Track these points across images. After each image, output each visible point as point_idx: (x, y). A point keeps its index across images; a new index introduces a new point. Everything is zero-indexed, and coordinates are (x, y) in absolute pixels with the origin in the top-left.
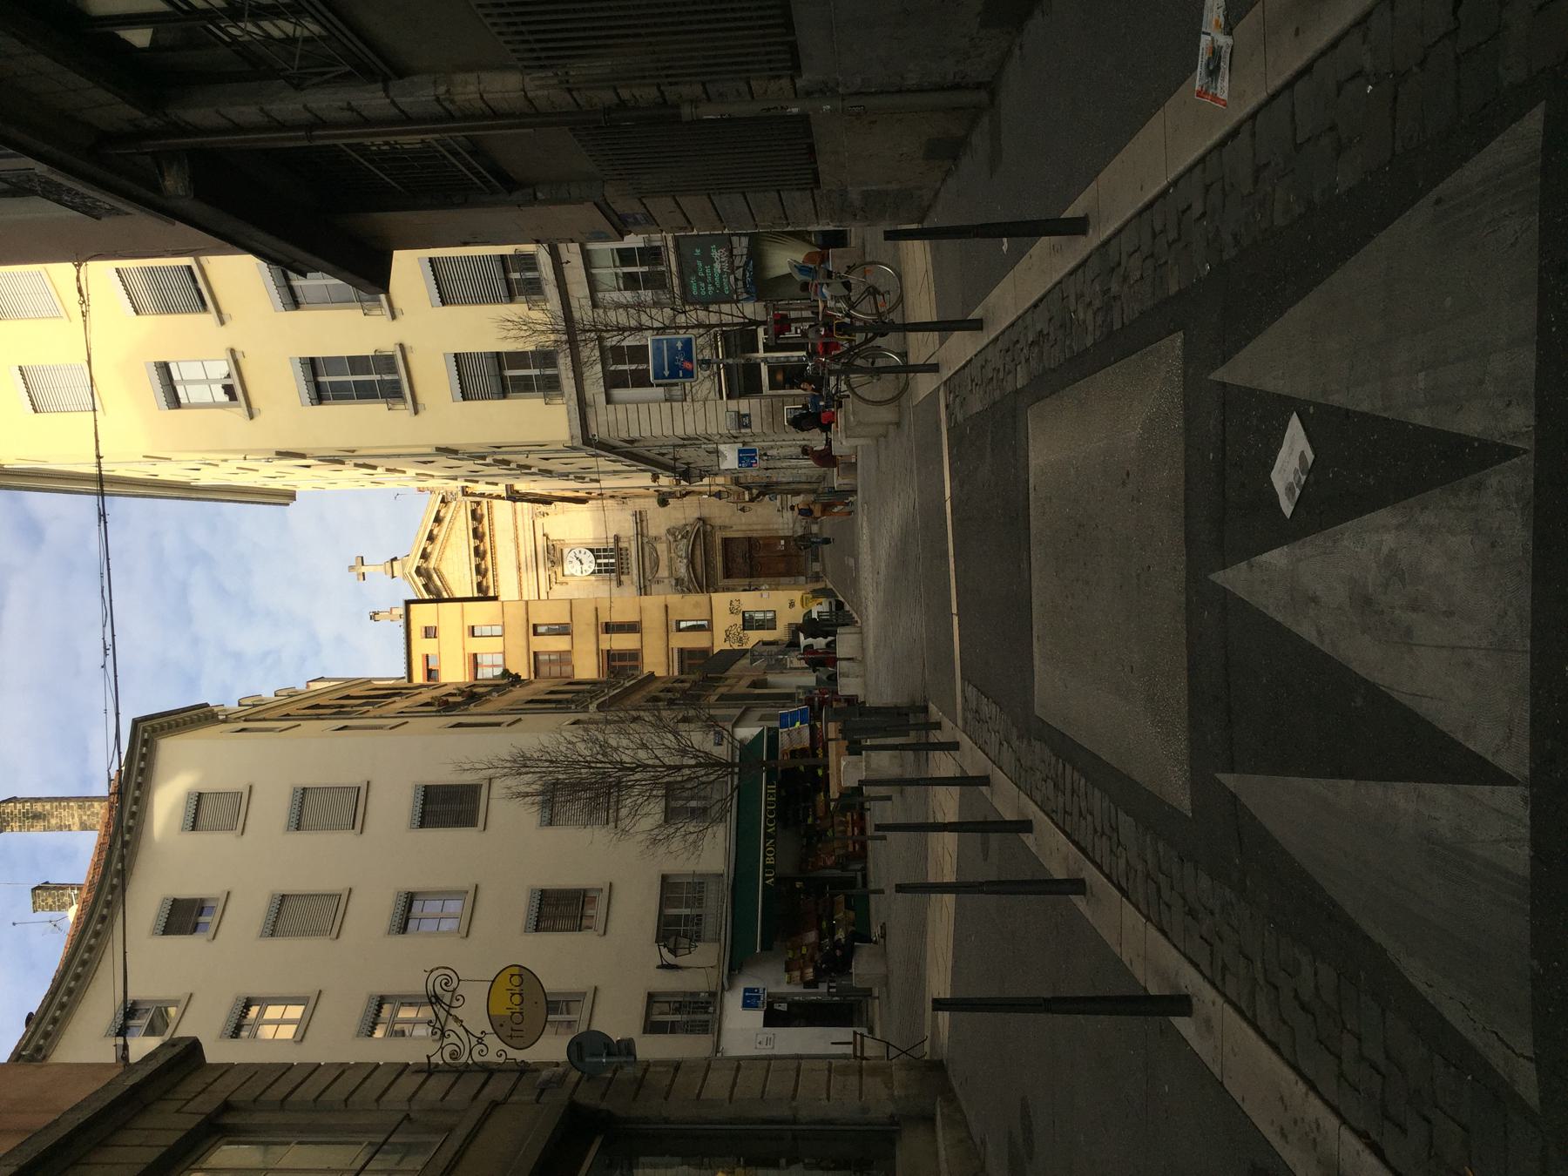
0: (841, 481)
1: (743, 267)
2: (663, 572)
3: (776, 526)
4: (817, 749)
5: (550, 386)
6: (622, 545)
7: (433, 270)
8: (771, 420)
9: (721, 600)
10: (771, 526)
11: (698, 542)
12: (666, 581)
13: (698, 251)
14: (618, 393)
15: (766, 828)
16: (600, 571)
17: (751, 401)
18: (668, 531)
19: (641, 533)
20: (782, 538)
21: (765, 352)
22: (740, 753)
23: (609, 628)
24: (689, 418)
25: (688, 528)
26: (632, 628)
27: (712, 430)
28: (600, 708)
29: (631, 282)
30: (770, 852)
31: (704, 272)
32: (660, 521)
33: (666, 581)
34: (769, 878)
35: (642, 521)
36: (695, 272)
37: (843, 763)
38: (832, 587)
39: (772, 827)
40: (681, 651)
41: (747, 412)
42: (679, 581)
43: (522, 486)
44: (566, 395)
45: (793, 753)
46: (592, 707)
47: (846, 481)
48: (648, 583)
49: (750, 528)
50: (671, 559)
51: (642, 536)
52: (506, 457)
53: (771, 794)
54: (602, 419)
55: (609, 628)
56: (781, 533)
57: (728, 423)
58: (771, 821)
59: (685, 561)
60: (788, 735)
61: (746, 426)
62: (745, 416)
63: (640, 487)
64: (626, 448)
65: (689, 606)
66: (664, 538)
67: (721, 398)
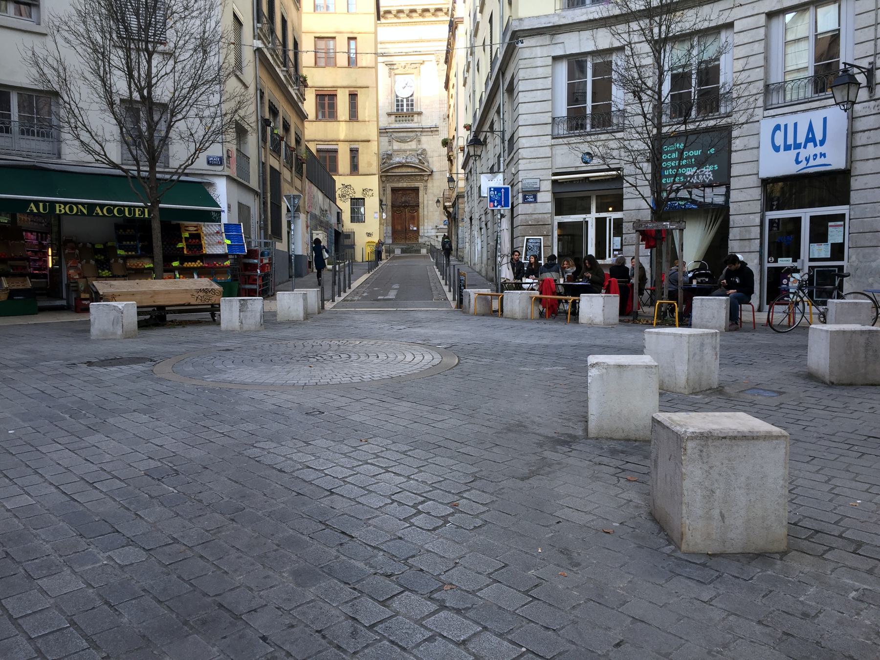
0: (473, 297)
1: (691, 198)
2: (396, 146)
3: (426, 224)
4: (202, 261)
6: (416, 116)
8: (530, 223)
9: (373, 183)
10: (426, 221)
11: (417, 170)
12: (390, 148)
14: (563, 68)
15: (102, 206)
16: (398, 101)
17: (550, 204)
18: (424, 150)
19: (423, 130)
20: (418, 228)
22: (166, 180)
23: (353, 96)
24: (535, 141)
25: (426, 164)
26: (353, 115)
27: (522, 165)
28: (258, 50)
29: (680, 80)
30: (71, 209)
32: (432, 146)
33: (390, 148)
34: (38, 208)
35: (432, 131)
37: (120, 305)
38: (380, 266)
39: (102, 212)
40: (336, 151)
41: (538, 200)
42: (389, 156)
43: (463, 32)
44: (564, 13)
45: (196, 237)
46: (259, 44)
47: (472, 301)
48: (389, 135)
49: (425, 208)
50: (405, 151)
51: (421, 131)
52: (471, 70)
53: (143, 213)
54: (538, 52)
55: (353, 96)
56: (421, 228)
57: (528, 181)
59: (404, 161)
60: (218, 232)
61: (524, 198)
62: (535, 197)
63: (457, 123)
64: (503, 85)
65: (369, 159)
66: (419, 147)
67: (555, 174)
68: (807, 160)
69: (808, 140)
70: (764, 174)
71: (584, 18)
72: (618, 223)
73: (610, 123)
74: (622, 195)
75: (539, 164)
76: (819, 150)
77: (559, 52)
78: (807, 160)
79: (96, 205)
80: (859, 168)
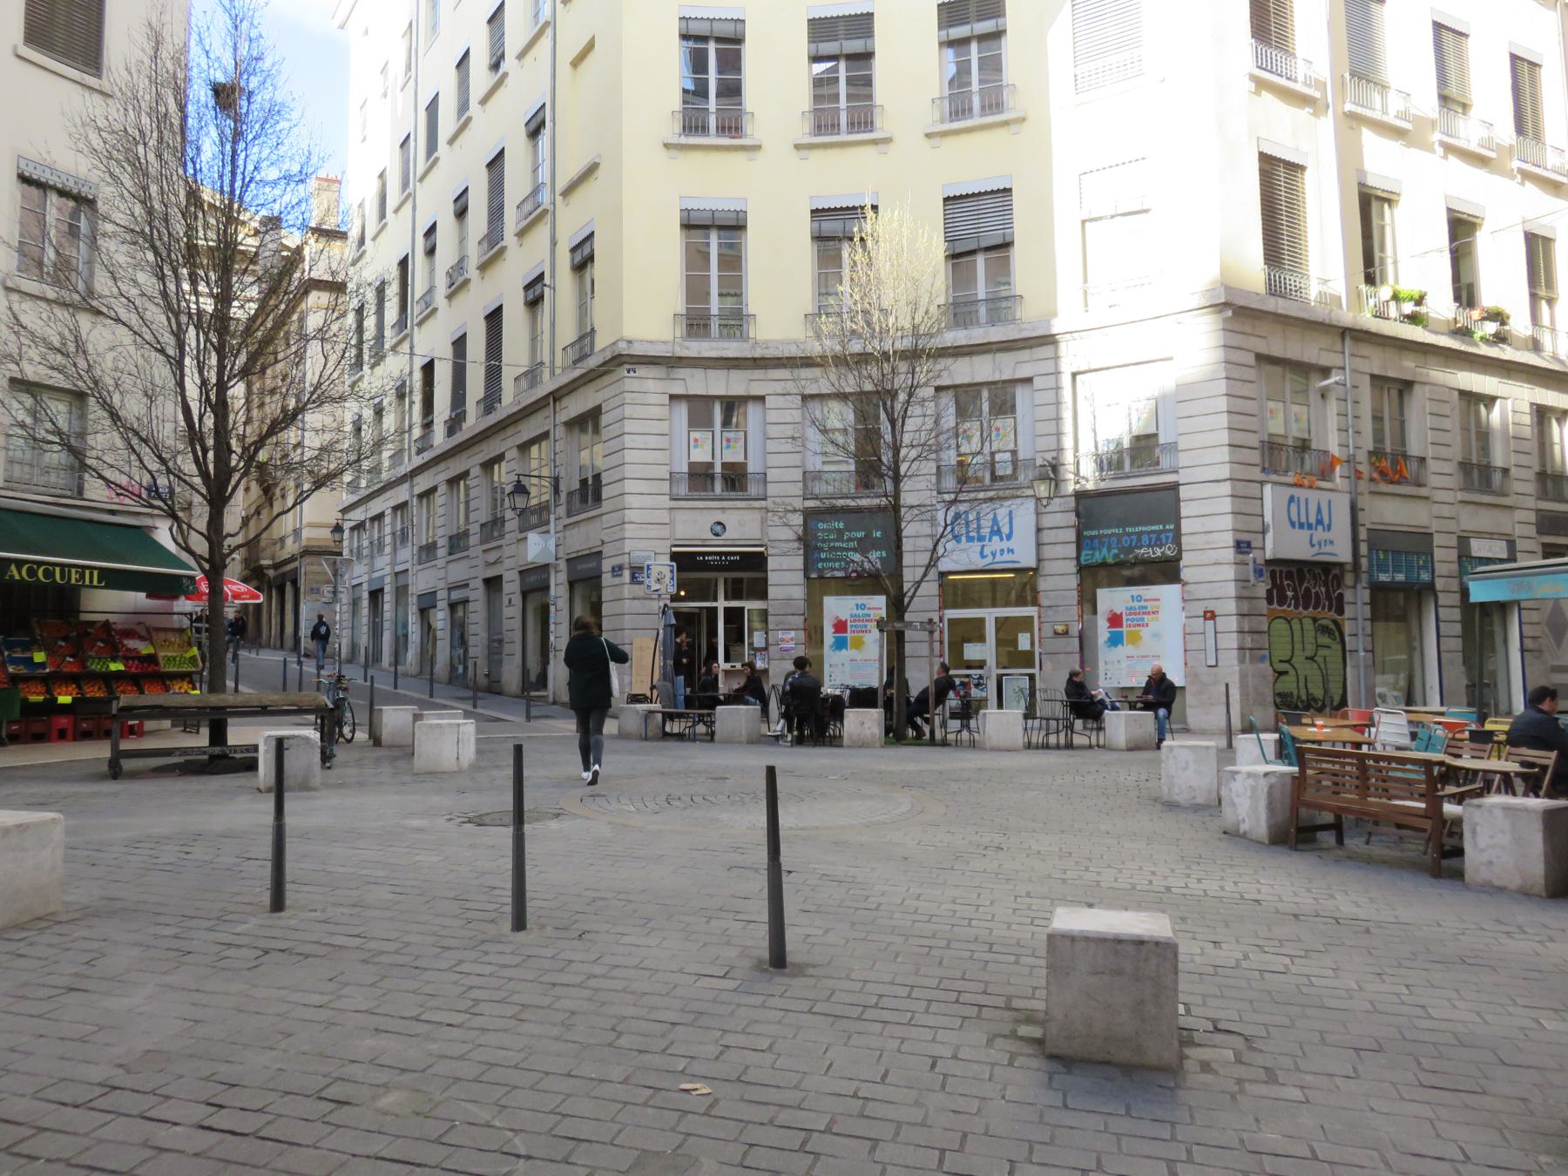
5: (696, 323)
7: (992, 192)
13: (878, 534)
15: (20, 563)
21: (981, 621)
31: (850, 539)
36: (848, 528)
39: (20, 573)
44: (686, 344)
53: (82, 576)
54: (651, 385)
58: (31, 572)
68: (994, 555)
69: (993, 533)
70: (1176, 588)
71: (714, 354)
72: (764, 614)
73: (744, 488)
74: (766, 580)
75: (654, 532)
76: (1005, 545)
77: (678, 389)
78: (994, 555)
79: (10, 561)
80: (1048, 567)
